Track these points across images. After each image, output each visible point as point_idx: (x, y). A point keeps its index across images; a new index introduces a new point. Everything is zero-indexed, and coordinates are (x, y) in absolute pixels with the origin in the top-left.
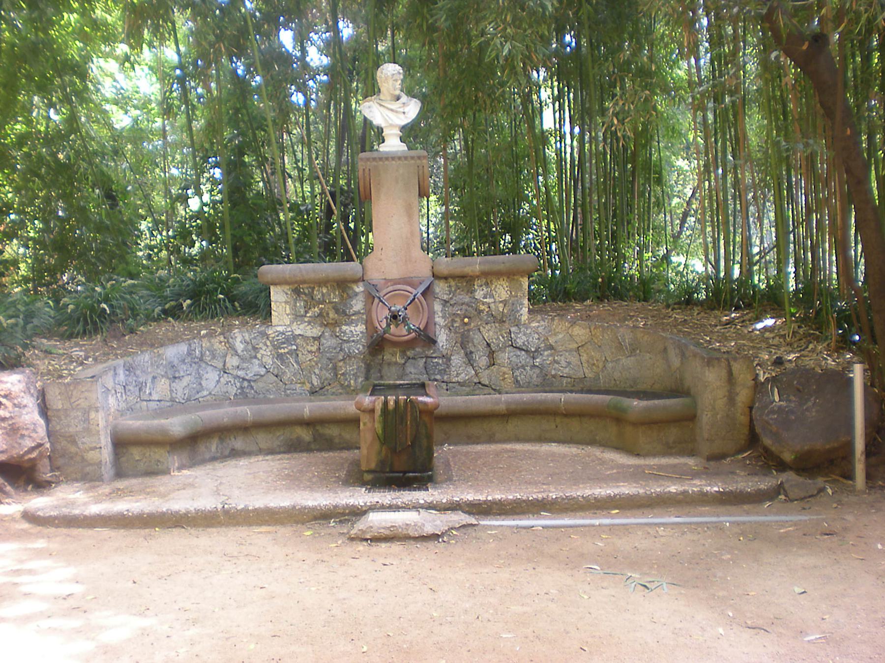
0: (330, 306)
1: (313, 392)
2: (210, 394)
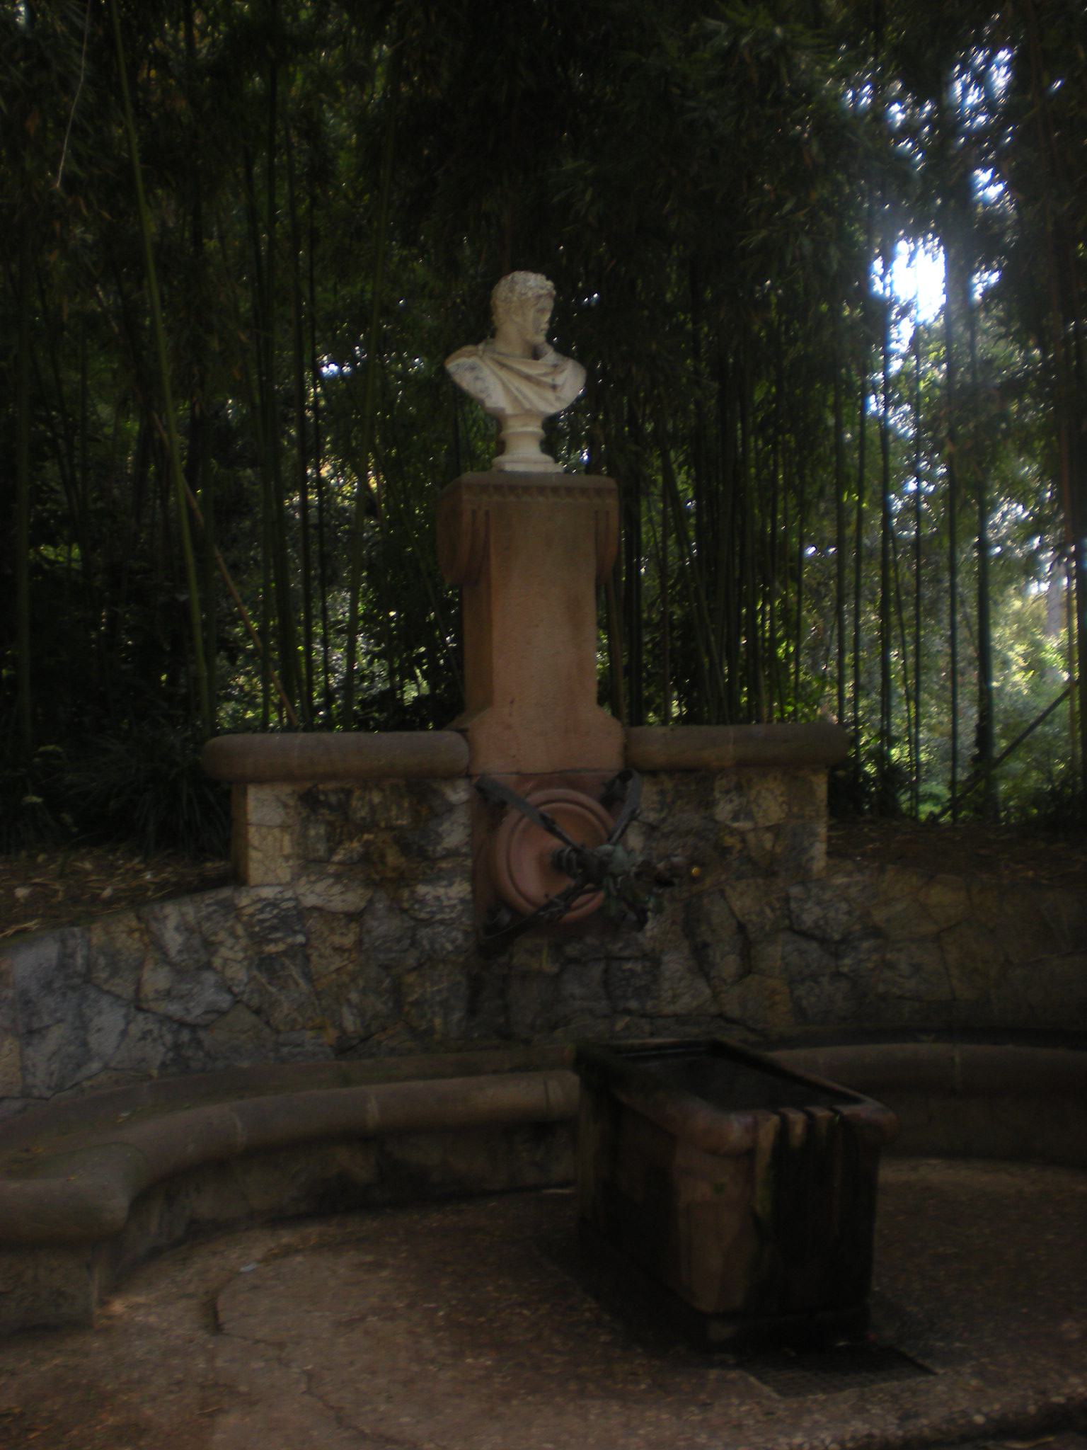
1: (344, 1048)
2: (106, 1067)
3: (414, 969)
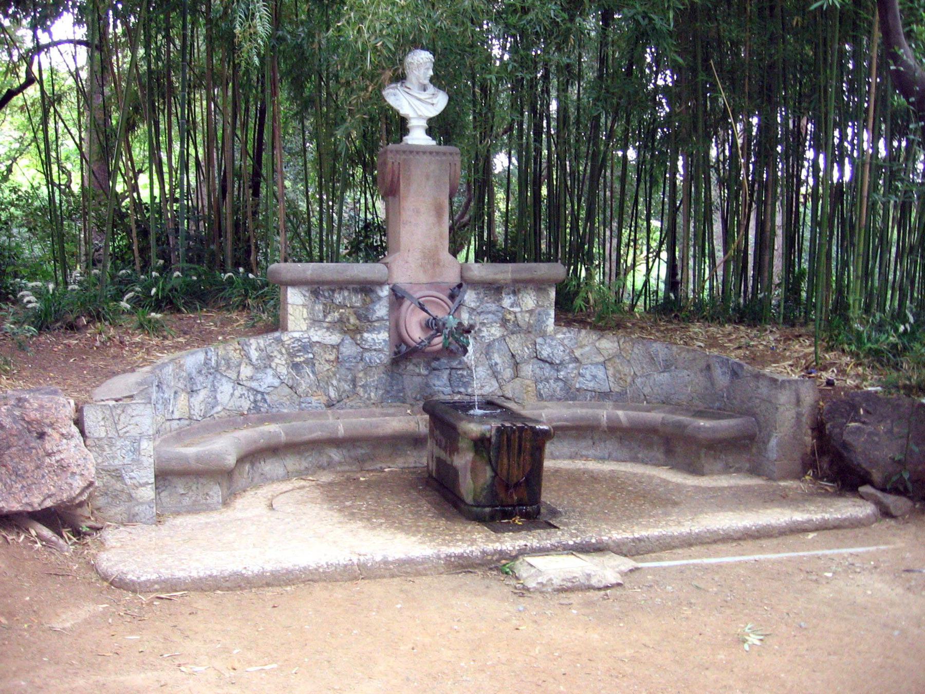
0: (351, 311)
1: (330, 405)
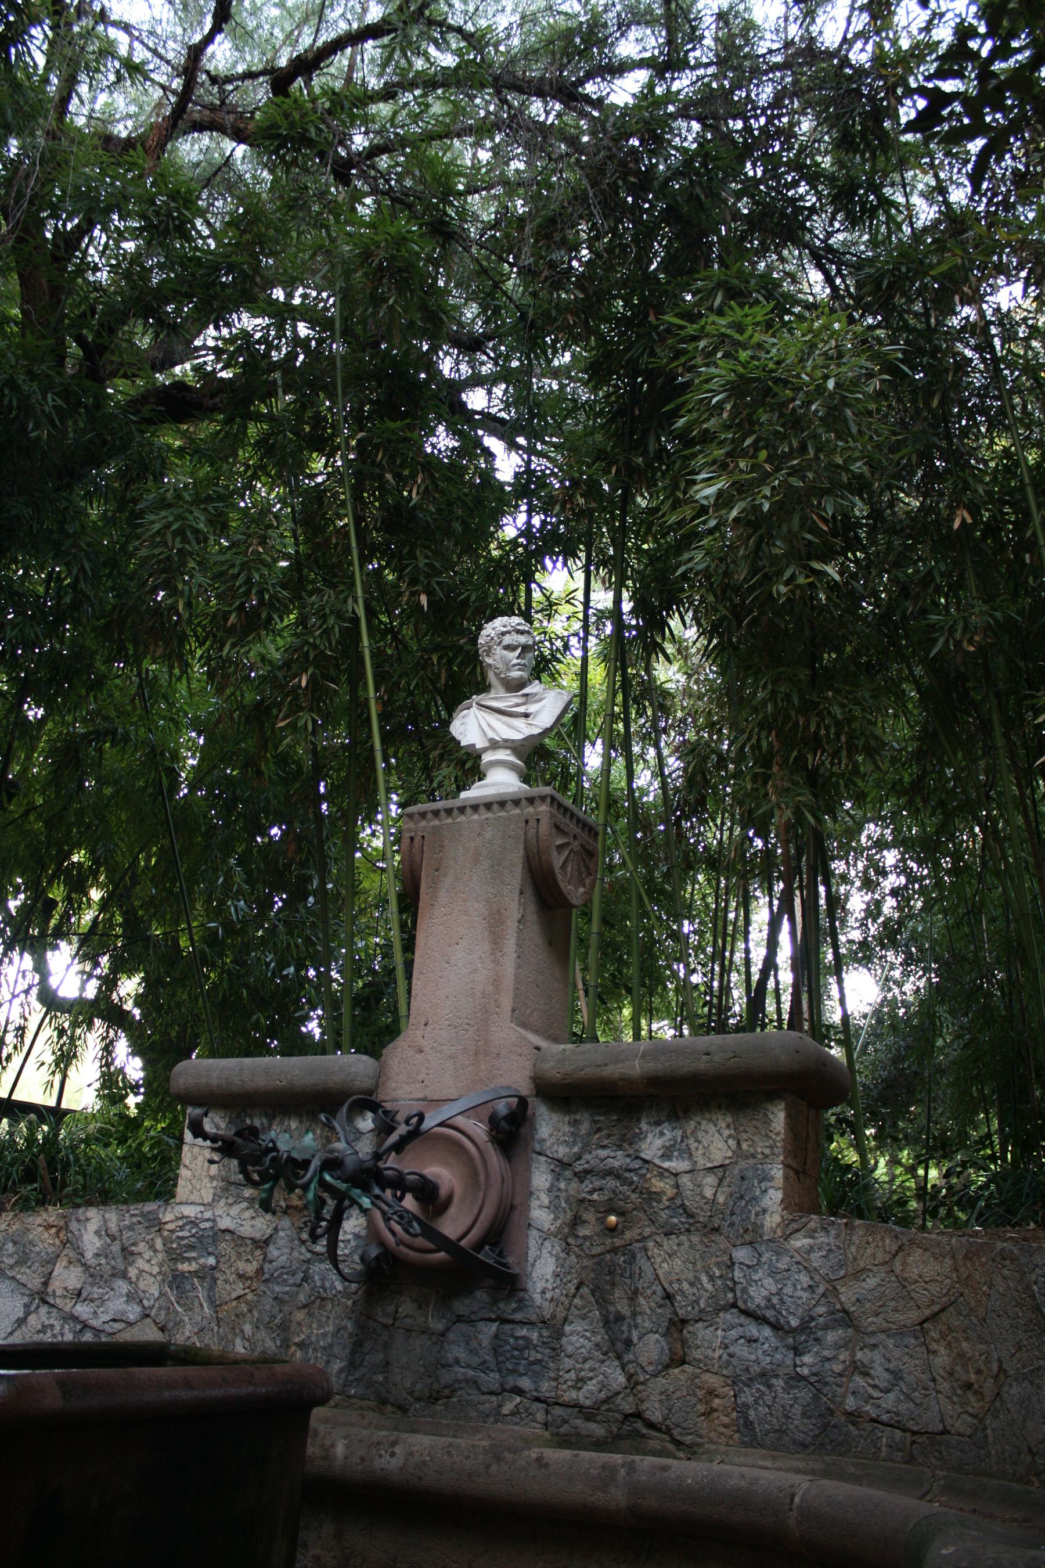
3: (305, 1306)
